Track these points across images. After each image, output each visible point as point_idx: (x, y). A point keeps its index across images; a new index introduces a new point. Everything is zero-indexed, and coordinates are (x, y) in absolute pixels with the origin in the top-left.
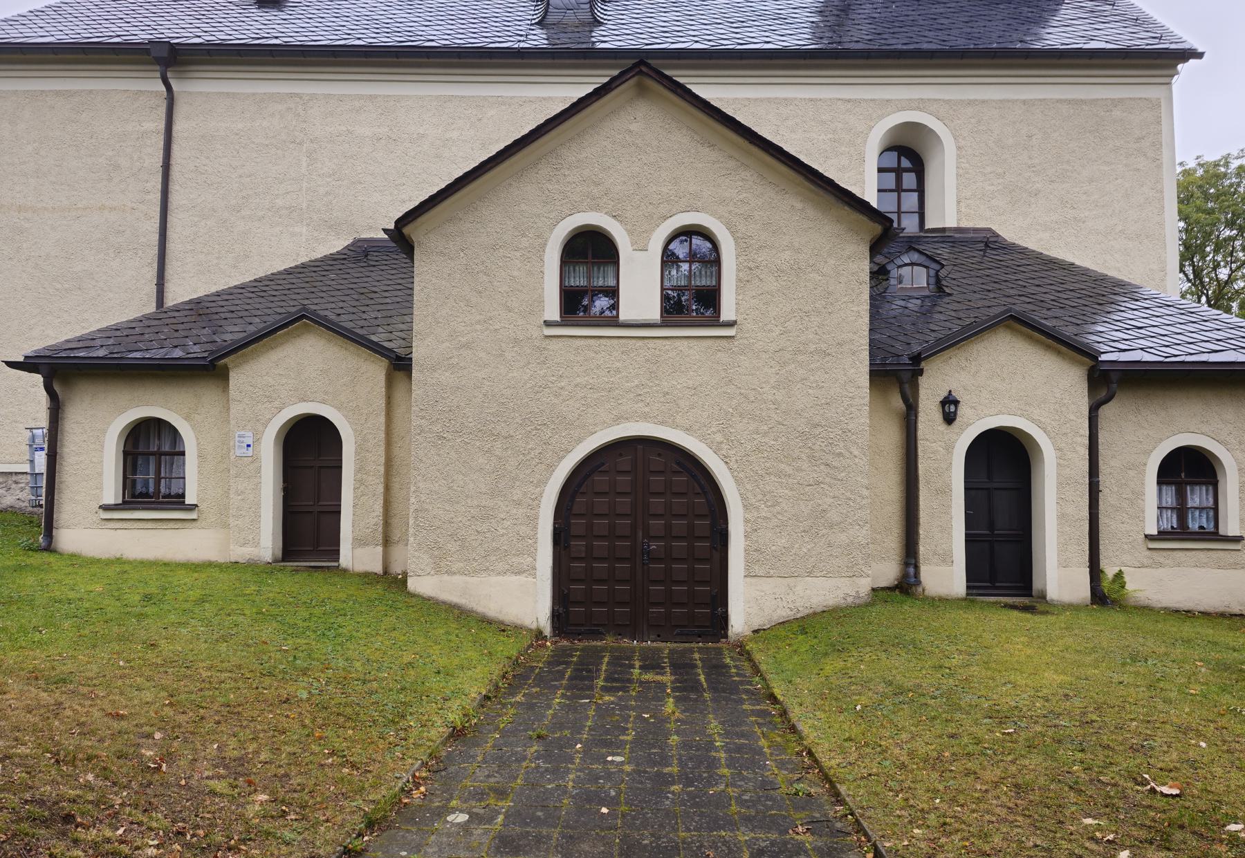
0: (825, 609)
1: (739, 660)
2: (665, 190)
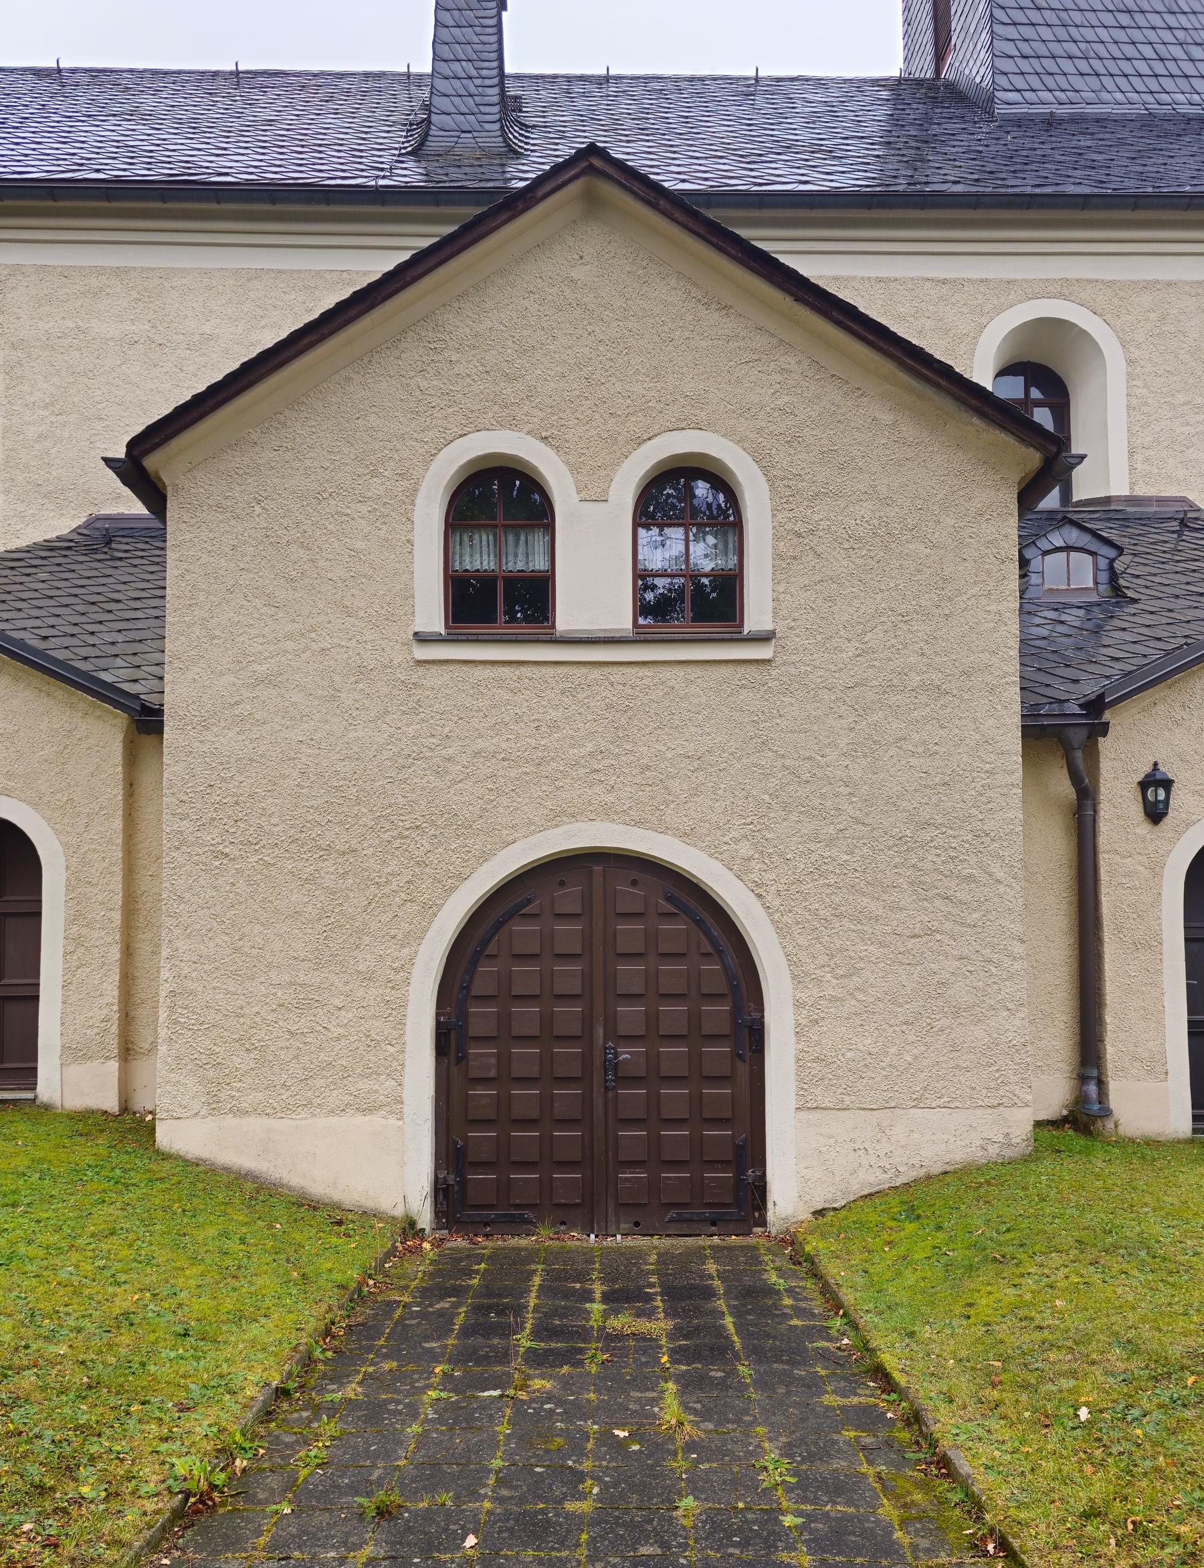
0: (948, 1169)
1: (794, 1275)
2: (638, 389)
